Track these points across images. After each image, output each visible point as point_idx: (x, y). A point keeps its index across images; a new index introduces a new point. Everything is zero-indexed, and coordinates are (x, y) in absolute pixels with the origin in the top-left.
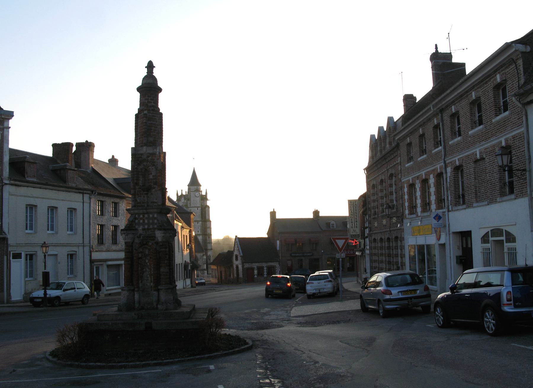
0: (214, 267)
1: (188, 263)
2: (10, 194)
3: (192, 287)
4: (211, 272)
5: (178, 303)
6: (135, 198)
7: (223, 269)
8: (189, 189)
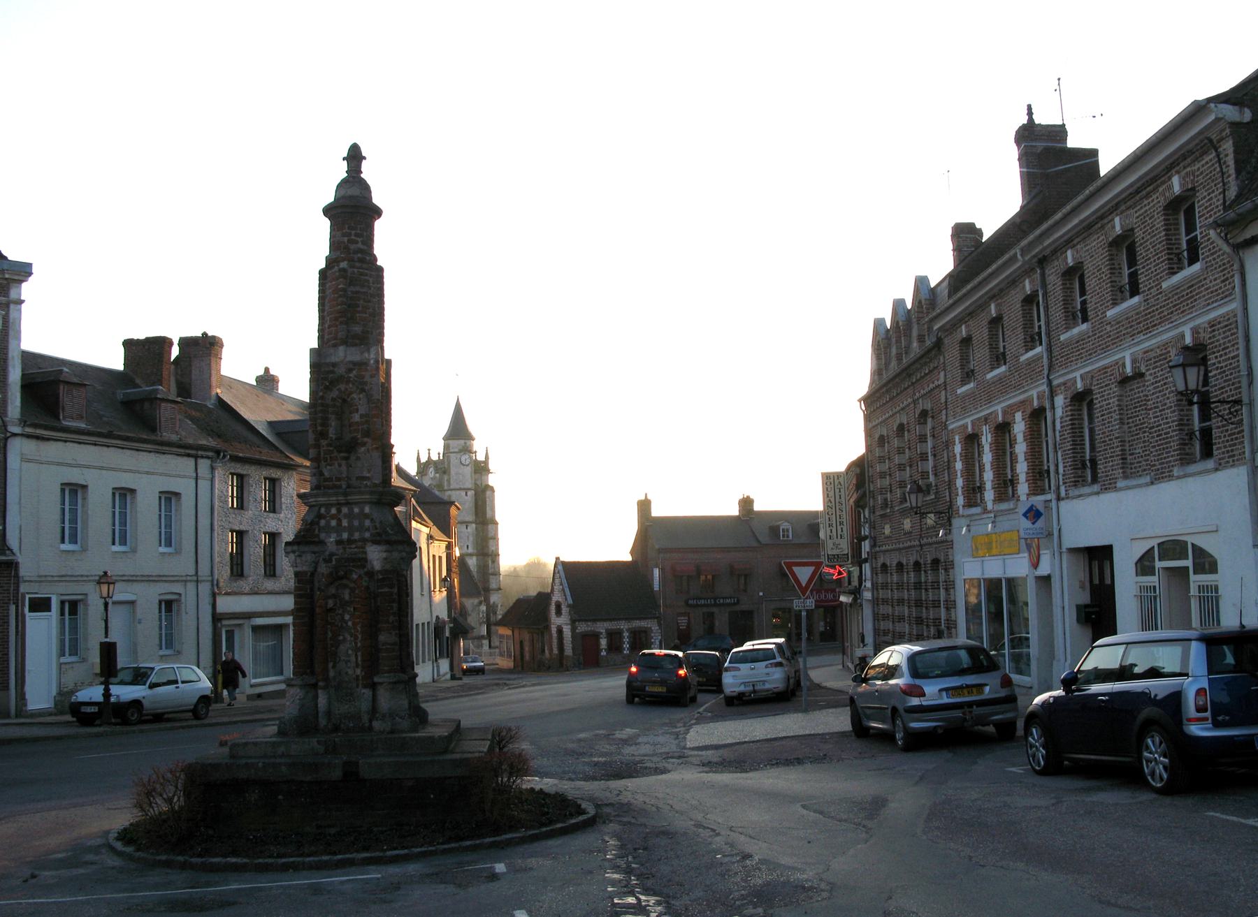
0: (503, 631)
1: (444, 622)
2: (25, 459)
3: (453, 678)
4: (497, 644)
5: (420, 717)
7: (526, 636)
8: (446, 447)
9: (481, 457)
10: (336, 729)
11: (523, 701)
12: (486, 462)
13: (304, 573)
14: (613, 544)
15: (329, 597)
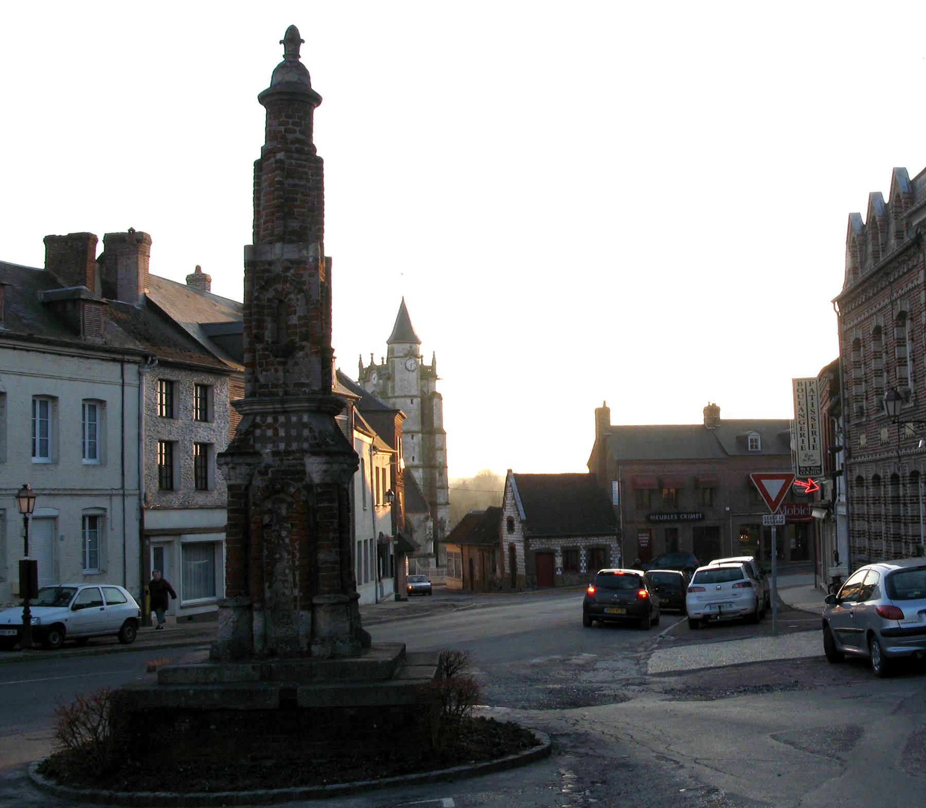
1: (388, 539)
3: (398, 599)
4: (445, 562)
5: (362, 640)
7: (476, 554)
8: (391, 352)
9: (427, 362)
10: (272, 653)
14: (571, 456)
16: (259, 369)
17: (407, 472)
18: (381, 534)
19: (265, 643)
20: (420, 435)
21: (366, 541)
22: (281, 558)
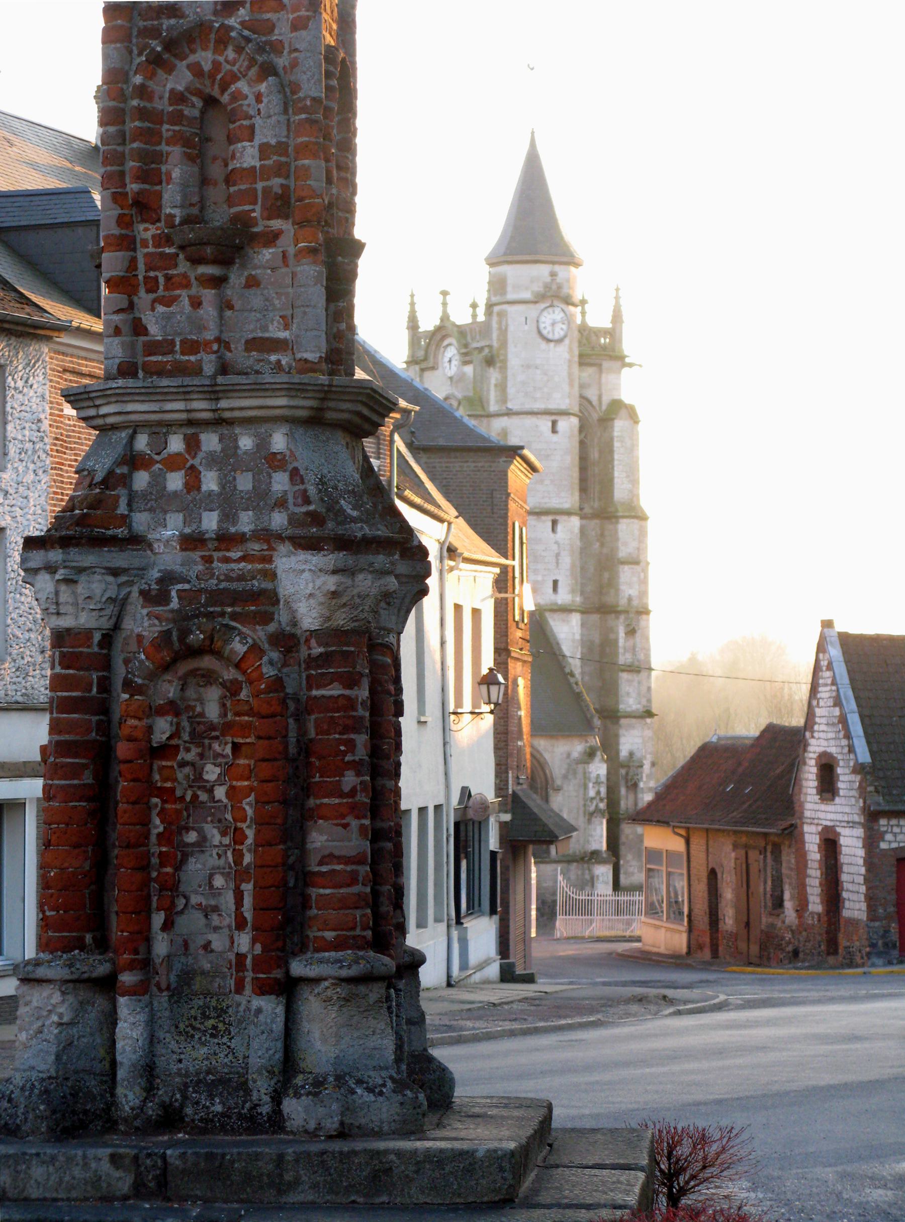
0: (662, 840)
1: (484, 807)
3: (508, 975)
4: (639, 877)
5: (427, 1086)
6: (131, 306)
7: (728, 858)
8: (498, 285)
9: (598, 317)
10: (170, 1119)
11: (720, 1052)
12: (613, 333)
13: (80, 636)
15: (161, 711)
16: (143, 297)
17: (538, 625)
18: (466, 793)
19: (150, 1090)
20: (575, 522)
21: (422, 810)
22: (202, 843)
